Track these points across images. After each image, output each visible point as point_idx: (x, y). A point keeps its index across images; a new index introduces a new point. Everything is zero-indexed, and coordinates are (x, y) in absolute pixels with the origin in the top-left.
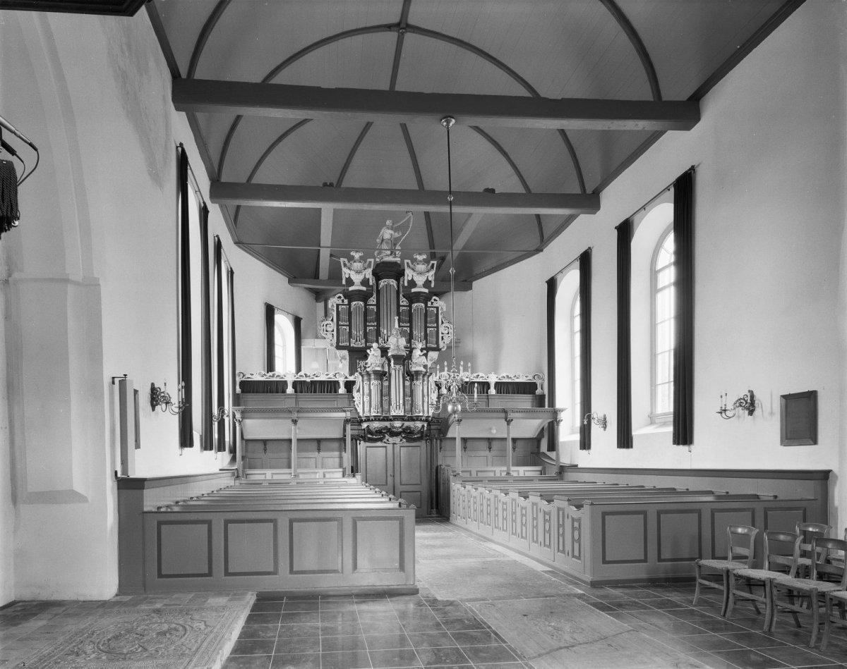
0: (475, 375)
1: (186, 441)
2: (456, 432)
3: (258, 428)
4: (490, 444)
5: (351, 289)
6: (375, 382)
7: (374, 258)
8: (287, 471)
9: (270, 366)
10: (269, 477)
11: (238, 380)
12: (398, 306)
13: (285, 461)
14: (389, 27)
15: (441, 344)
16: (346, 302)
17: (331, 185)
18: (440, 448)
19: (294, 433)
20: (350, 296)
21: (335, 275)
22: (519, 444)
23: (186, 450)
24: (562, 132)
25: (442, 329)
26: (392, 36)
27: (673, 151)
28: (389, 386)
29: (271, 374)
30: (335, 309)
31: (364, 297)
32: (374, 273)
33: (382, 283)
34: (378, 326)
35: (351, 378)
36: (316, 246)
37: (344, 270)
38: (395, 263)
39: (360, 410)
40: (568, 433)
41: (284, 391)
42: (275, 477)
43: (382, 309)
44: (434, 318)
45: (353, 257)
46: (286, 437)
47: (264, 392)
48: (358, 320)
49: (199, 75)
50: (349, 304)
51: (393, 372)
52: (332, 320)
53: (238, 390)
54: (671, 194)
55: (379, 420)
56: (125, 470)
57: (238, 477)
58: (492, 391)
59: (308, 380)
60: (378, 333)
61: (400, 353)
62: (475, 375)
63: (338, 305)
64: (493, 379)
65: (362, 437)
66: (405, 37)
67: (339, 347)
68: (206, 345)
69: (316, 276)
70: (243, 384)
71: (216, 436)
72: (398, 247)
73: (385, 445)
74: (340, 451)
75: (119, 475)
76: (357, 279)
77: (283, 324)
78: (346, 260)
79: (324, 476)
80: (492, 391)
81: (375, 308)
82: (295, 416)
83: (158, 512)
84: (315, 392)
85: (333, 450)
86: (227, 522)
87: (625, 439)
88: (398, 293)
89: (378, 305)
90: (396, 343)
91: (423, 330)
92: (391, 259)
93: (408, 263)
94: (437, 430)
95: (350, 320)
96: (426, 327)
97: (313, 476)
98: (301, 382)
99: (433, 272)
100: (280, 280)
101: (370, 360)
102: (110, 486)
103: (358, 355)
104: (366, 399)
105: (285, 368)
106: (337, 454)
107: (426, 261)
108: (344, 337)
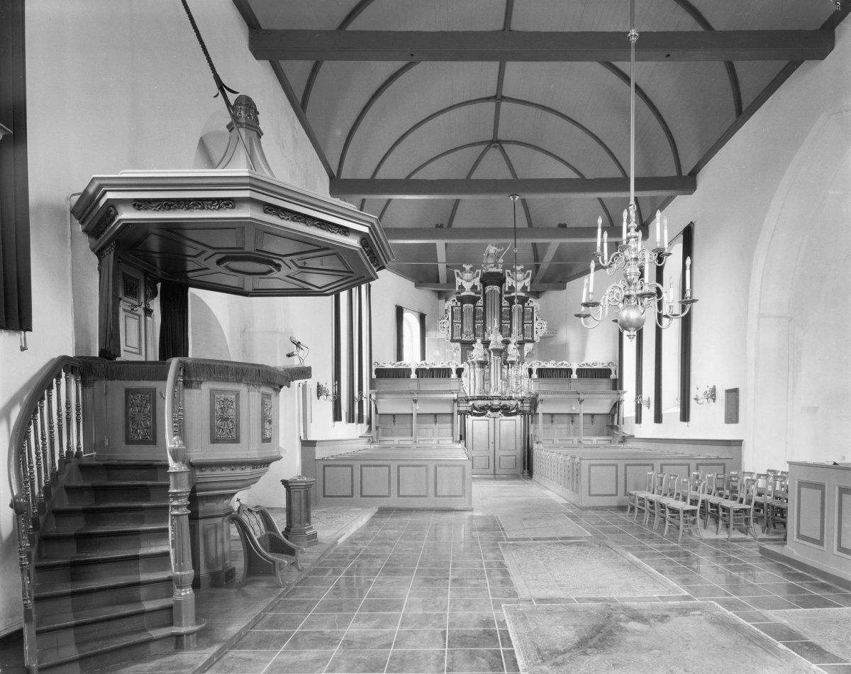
0: (560, 363)
1: (337, 417)
2: (541, 409)
3: (388, 406)
4: (573, 418)
5: (463, 294)
6: (478, 369)
7: (482, 269)
8: (410, 438)
9: (400, 357)
10: (396, 442)
11: (374, 368)
12: (501, 307)
13: (409, 430)
14: (488, 99)
15: (536, 337)
16: (459, 304)
17: (441, 226)
18: (532, 422)
19: (418, 408)
20: (462, 300)
21: (451, 280)
22: (596, 418)
23: (338, 423)
24: (600, 199)
25: (536, 325)
26: (492, 105)
27: (682, 208)
28: (490, 373)
29: (399, 363)
30: (450, 310)
31: (473, 300)
32: (481, 281)
33: (488, 289)
34: (485, 323)
35: (461, 366)
36: (434, 262)
37: (457, 279)
38: (498, 273)
39: (467, 391)
40: (628, 410)
41: (409, 377)
42: (401, 443)
43: (487, 309)
44: (530, 316)
45: (464, 269)
46: (410, 412)
47: (393, 377)
48: (468, 320)
49: (343, 176)
50: (462, 306)
51: (493, 362)
52: (448, 319)
53: (374, 376)
54: (681, 237)
55: (481, 399)
56: (305, 435)
57: (373, 442)
58: (574, 376)
59: (428, 367)
60: (484, 329)
61: (498, 347)
62: (560, 363)
63: (452, 307)
64: (575, 367)
65: (469, 412)
66: (502, 106)
67: (452, 341)
68: (350, 374)
69: (438, 281)
70: (378, 371)
71: (356, 411)
72: (501, 261)
73: (488, 418)
74: (568, 423)
75: (302, 438)
76: (467, 286)
77: (411, 323)
78: (458, 271)
79: (439, 442)
80: (574, 376)
81: (482, 308)
82: (416, 396)
83: (323, 459)
84: (433, 377)
85: (447, 422)
86: (362, 466)
87: (658, 418)
88: (501, 296)
89: (484, 306)
90: (496, 339)
91: (520, 325)
92: (495, 270)
93: (508, 273)
94: (529, 409)
95: (462, 321)
96: (523, 324)
97: (430, 442)
98: (422, 369)
99: (529, 280)
100: (410, 284)
101: (474, 353)
102: (298, 443)
103: (467, 346)
104: (472, 382)
105: (412, 359)
106: (566, 426)
107: (523, 271)
108: (457, 333)
